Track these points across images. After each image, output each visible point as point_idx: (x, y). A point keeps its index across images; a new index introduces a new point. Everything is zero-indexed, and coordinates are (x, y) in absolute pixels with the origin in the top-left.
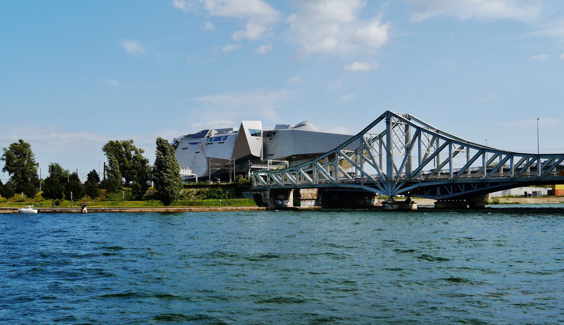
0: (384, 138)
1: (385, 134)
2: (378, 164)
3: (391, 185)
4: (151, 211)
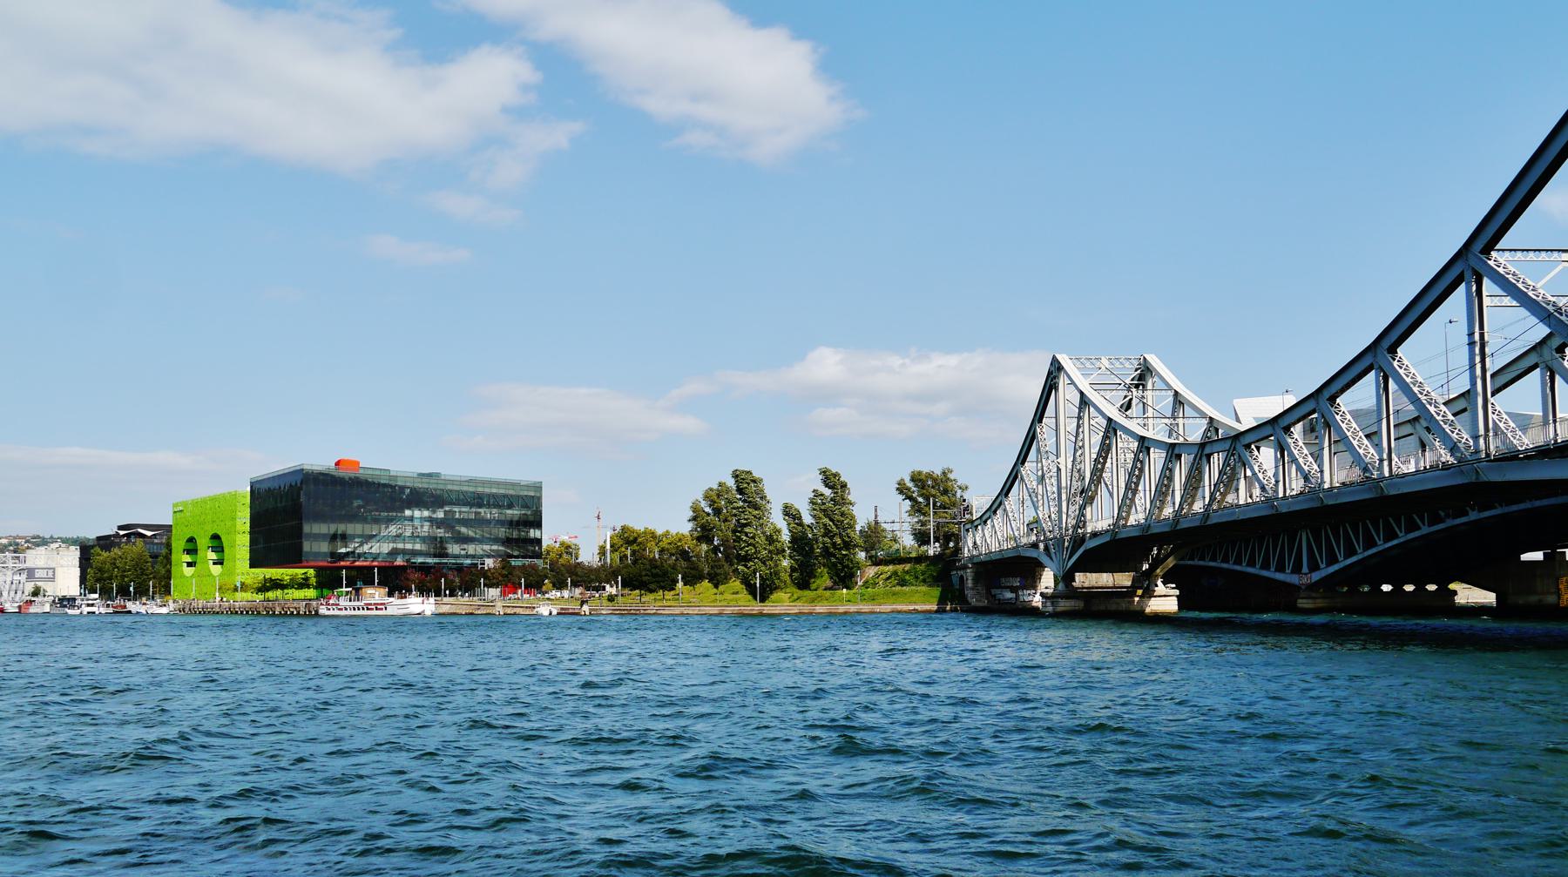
1: (1298, 421)
4: (696, 612)
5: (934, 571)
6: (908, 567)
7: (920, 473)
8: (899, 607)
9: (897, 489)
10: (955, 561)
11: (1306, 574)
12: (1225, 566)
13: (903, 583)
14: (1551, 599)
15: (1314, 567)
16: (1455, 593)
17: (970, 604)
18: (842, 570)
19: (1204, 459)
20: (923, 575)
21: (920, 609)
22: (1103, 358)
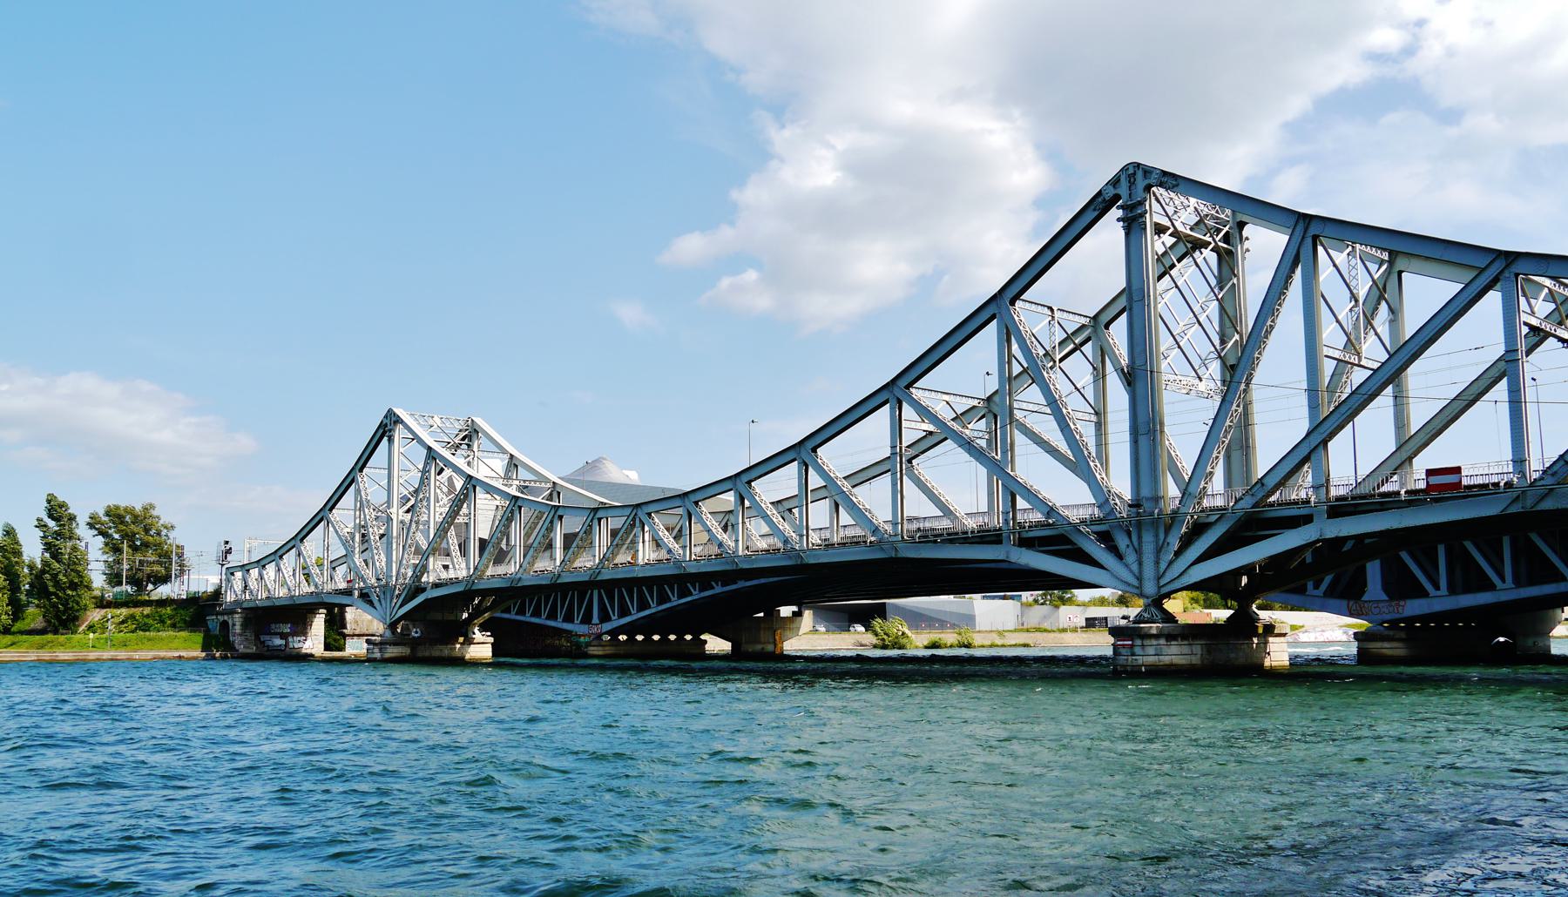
0: (1118, 333)
2: (1091, 441)
3: (1157, 536)
5: (186, 614)
6: (147, 610)
7: (117, 508)
8: (162, 654)
9: (88, 524)
10: (215, 606)
11: (597, 624)
12: (506, 616)
13: (145, 628)
14: (770, 648)
15: (605, 618)
16: (705, 642)
17: (238, 651)
18: (64, 612)
19: (596, 522)
20: (170, 619)
21: (186, 656)
22: (436, 416)
